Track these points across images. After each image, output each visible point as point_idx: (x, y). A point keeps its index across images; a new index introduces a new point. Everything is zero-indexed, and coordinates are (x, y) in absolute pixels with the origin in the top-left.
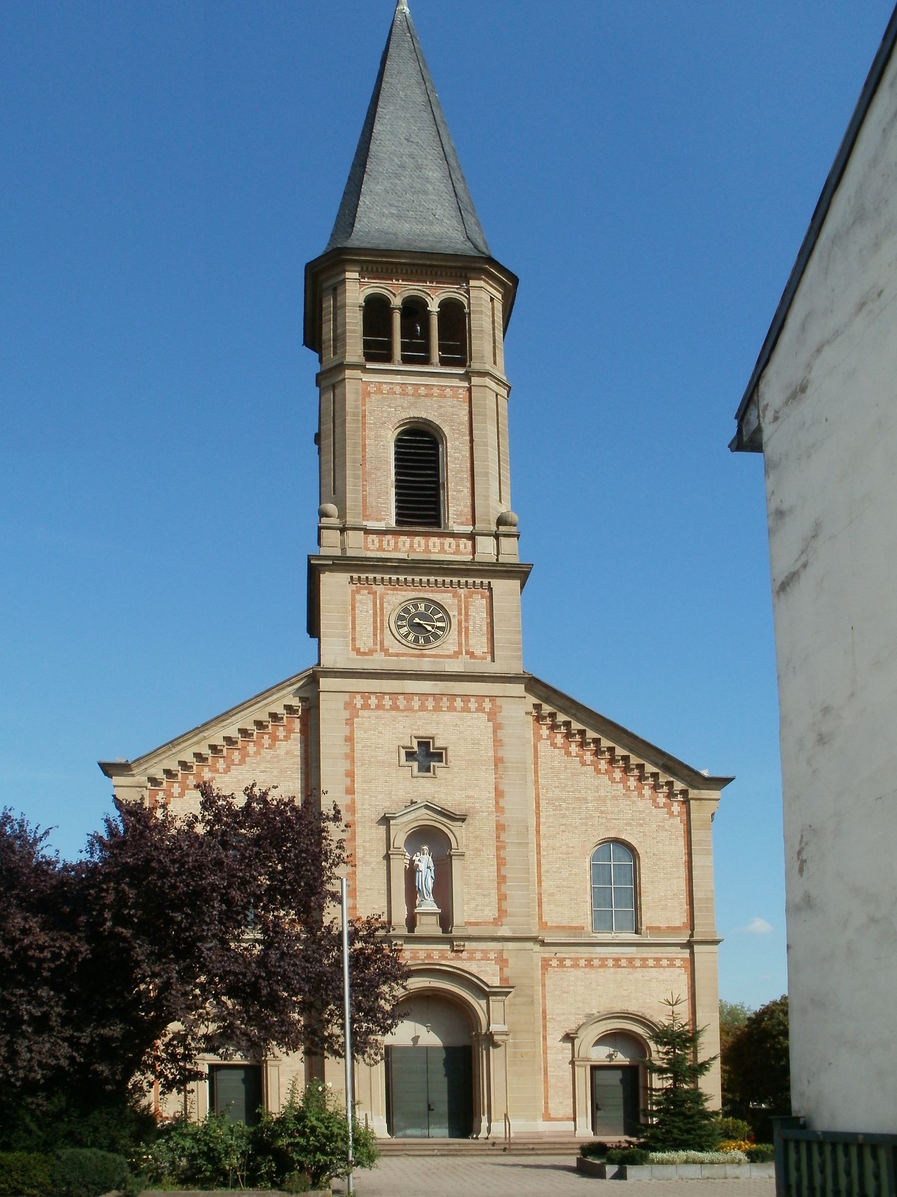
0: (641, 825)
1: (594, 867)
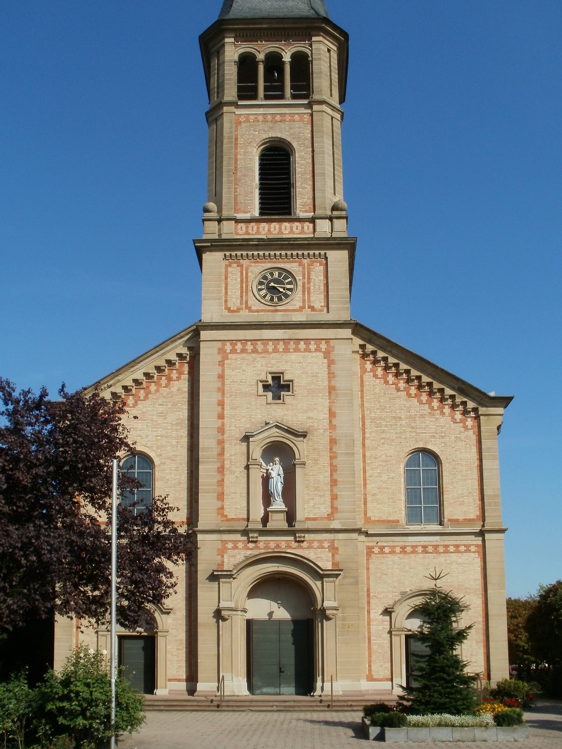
0: (443, 437)
1: (407, 472)
